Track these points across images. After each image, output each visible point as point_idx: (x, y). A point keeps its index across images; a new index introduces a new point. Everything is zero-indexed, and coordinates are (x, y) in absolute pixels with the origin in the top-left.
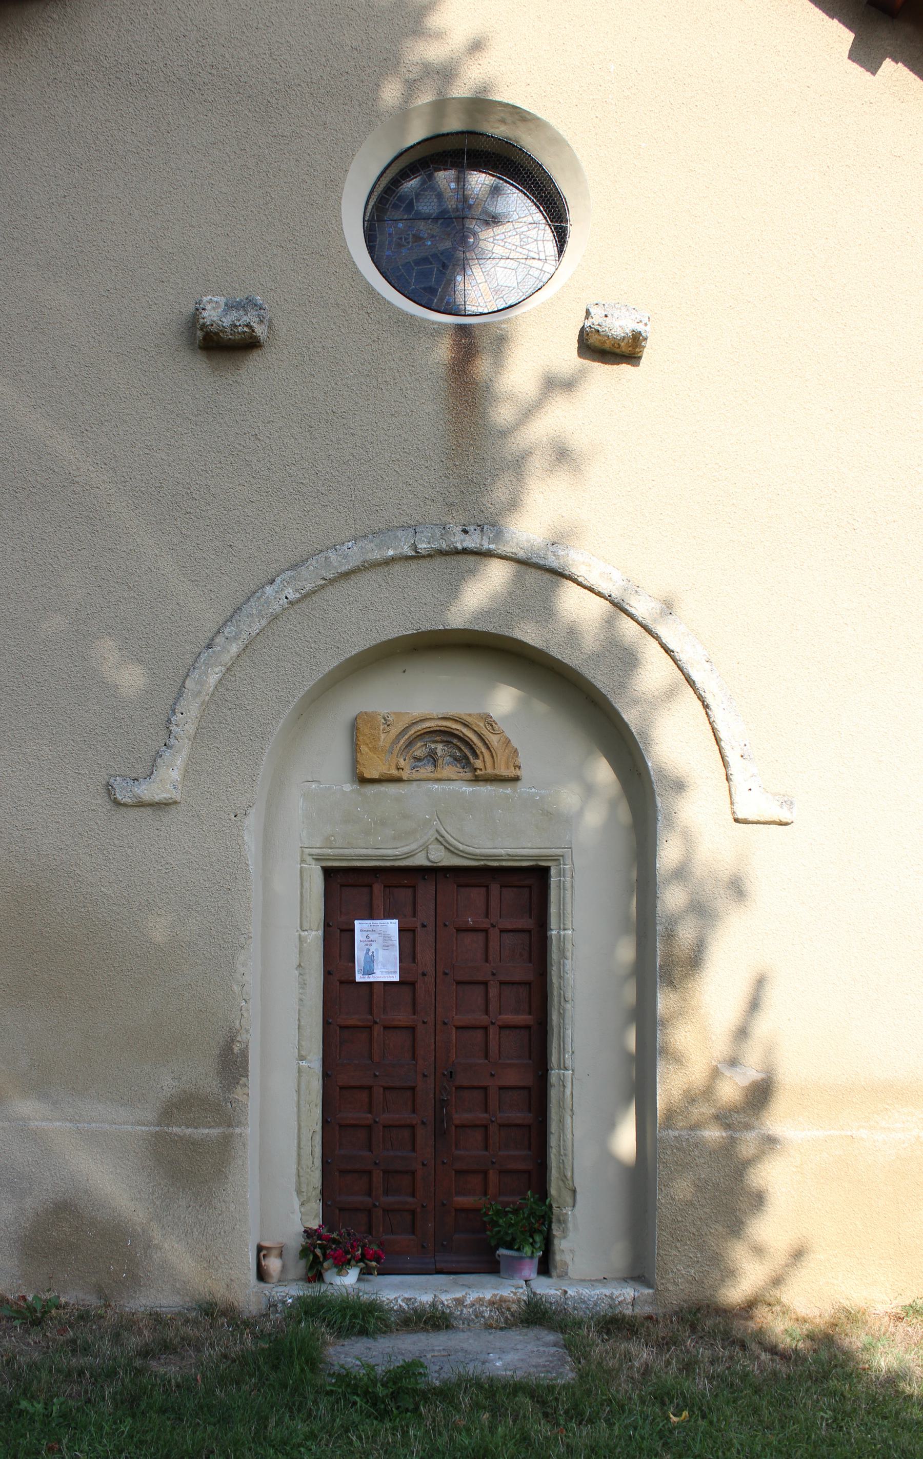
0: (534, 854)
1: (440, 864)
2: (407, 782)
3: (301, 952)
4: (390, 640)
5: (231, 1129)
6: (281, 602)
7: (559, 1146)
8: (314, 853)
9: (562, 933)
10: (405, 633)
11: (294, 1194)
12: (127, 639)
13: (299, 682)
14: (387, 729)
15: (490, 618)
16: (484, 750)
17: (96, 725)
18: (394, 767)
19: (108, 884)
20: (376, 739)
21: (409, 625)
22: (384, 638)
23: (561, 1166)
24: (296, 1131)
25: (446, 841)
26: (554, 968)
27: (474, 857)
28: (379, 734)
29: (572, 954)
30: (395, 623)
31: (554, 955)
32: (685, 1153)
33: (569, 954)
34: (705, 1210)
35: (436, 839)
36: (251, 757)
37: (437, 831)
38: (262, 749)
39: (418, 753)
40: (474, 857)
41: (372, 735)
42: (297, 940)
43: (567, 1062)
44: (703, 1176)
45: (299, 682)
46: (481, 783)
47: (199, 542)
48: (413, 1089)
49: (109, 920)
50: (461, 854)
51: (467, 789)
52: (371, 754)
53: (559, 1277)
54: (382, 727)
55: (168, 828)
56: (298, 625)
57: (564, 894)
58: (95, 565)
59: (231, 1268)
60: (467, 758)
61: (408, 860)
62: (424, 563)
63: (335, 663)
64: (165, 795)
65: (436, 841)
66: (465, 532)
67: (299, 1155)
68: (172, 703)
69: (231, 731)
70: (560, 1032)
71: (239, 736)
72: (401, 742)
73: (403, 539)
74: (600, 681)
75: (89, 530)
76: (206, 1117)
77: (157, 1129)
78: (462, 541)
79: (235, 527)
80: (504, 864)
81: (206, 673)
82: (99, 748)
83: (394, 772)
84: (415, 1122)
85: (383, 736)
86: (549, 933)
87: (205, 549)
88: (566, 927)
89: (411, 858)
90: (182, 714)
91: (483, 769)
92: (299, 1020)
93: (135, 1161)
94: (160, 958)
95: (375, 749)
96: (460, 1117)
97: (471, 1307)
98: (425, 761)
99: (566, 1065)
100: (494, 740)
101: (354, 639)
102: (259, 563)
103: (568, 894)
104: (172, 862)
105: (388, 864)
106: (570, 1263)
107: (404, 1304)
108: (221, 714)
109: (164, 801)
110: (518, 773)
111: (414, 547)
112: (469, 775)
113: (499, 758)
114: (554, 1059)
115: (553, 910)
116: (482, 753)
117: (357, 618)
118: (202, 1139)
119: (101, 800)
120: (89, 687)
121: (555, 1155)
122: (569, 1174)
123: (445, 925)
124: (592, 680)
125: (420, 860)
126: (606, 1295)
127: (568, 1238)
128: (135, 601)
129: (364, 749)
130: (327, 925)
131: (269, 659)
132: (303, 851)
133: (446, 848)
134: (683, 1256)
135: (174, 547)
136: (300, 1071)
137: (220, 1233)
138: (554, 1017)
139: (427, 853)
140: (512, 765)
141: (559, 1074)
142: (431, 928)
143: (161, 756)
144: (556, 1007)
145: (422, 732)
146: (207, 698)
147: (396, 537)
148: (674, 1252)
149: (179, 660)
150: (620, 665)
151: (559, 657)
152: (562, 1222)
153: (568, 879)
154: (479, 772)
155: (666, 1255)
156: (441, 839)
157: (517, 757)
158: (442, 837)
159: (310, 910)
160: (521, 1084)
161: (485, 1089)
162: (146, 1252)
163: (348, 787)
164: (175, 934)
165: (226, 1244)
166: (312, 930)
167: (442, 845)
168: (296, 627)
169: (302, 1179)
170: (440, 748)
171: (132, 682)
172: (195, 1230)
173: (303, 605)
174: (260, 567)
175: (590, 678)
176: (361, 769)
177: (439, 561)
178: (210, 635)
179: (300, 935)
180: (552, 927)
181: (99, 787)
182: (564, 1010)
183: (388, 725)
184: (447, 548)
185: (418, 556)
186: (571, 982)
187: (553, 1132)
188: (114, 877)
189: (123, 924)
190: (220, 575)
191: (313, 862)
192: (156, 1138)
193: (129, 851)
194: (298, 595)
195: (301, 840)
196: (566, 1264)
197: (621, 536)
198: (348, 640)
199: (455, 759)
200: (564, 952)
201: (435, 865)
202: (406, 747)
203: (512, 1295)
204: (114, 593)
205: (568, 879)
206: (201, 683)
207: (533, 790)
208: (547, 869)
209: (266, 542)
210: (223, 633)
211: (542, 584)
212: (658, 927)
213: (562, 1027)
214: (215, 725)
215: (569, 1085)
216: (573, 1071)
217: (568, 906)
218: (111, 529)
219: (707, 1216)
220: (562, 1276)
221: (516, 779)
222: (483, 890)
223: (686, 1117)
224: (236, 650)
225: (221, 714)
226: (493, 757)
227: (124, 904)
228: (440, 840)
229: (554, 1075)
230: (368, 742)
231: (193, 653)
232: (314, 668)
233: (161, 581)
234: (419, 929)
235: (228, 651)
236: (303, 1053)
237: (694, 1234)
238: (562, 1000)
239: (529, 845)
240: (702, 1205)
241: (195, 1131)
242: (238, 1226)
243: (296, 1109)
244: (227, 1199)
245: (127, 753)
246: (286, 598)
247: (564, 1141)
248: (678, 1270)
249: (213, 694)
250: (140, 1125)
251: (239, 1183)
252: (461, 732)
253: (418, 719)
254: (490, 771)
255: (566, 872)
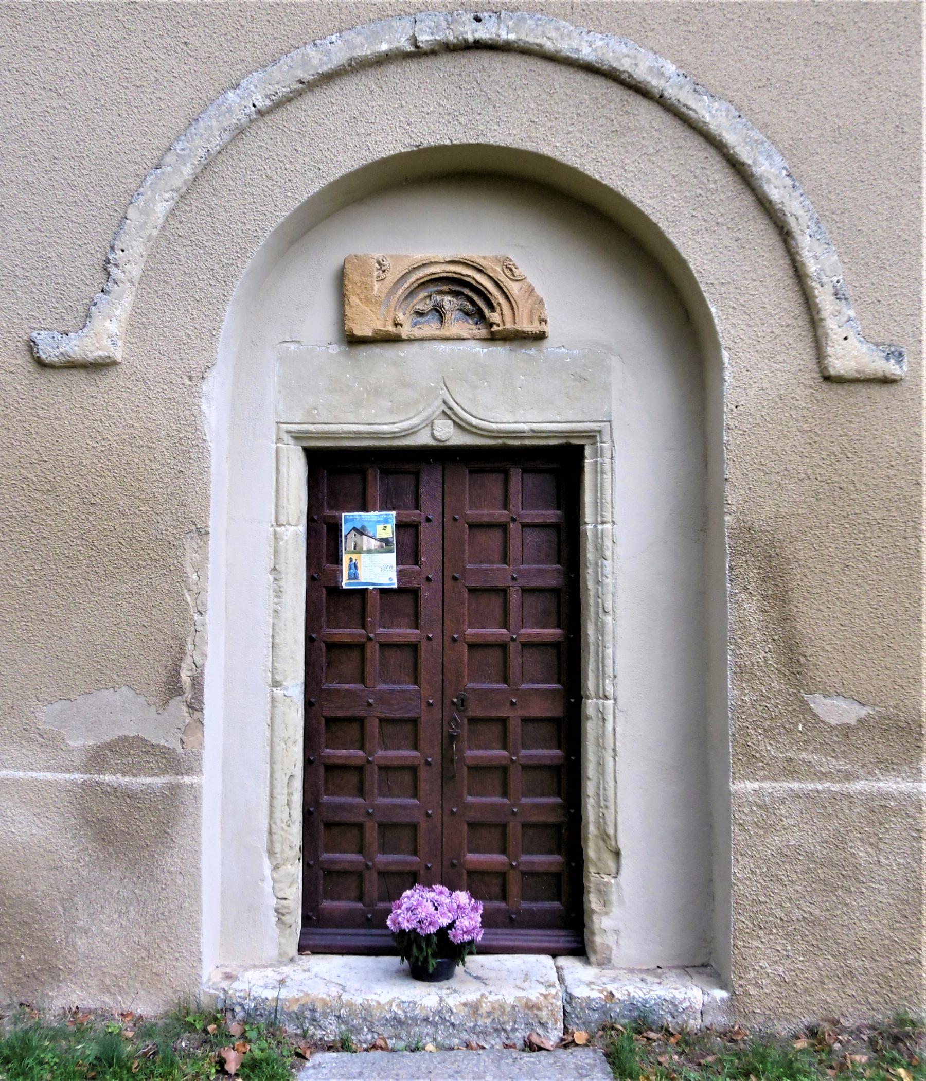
0: (564, 429)
1: (448, 443)
2: (406, 343)
3: (276, 552)
4: (384, 161)
5: (180, 777)
6: (247, 111)
7: (598, 795)
8: (292, 429)
9: (600, 527)
10: (403, 151)
11: (265, 855)
12: (55, 158)
13: (271, 213)
14: (382, 276)
15: (509, 129)
16: (502, 300)
17: (17, 265)
18: (390, 322)
19: (28, 465)
20: (368, 288)
21: (407, 140)
22: (376, 157)
23: (601, 820)
24: (268, 776)
25: (456, 414)
26: (590, 571)
27: (489, 434)
28: (372, 281)
29: (613, 553)
30: (390, 138)
31: (590, 553)
32: (768, 812)
33: (608, 553)
34: (797, 887)
35: (444, 412)
36: (210, 307)
37: (445, 402)
38: (224, 295)
39: (420, 307)
40: (490, 434)
41: (363, 283)
42: (272, 537)
43: (607, 689)
44: (793, 843)
45: (271, 213)
46: (499, 343)
47: (145, 39)
48: (415, 722)
49: (29, 509)
50: (474, 430)
51: (481, 350)
52: (363, 307)
53: (600, 964)
54: (376, 273)
55: (105, 395)
56: (269, 141)
57: (602, 479)
58: (16, 66)
59: (177, 959)
60: (480, 313)
61: (408, 438)
62: (426, 63)
63: (315, 188)
64: (100, 353)
65: (442, 416)
66: (478, 20)
67: (271, 806)
68: (111, 238)
69: (185, 273)
70: (598, 651)
71: (196, 279)
72: (400, 292)
73: (400, 30)
74: (649, 206)
75: (9, 23)
76: (149, 762)
77: (86, 777)
78: (474, 31)
79: (191, 19)
80: (527, 442)
81: (153, 200)
82: (19, 294)
83: (391, 328)
84: (417, 762)
85: (377, 285)
86: (582, 528)
87: (154, 47)
88: (605, 519)
89: (413, 436)
90: (123, 251)
91: (501, 325)
92: (273, 636)
93: (56, 818)
94: (93, 559)
95: (367, 300)
96: (474, 754)
97: (488, 1016)
98: (430, 317)
99: (607, 694)
100: (514, 288)
101: (339, 158)
102: (221, 63)
103: (607, 478)
104: (110, 438)
105: (384, 443)
106: (614, 947)
107: (399, 1012)
108: (173, 252)
109: (100, 361)
110: (543, 327)
111: (414, 41)
112: (483, 332)
113: (520, 309)
114: (590, 684)
115: (588, 497)
116: (499, 304)
117: (343, 132)
118: (142, 791)
119: (23, 360)
120: (8, 218)
121: (593, 806)
122: (611, 831)
123: (455, 519)
124: (639, 205)
125: (423, 439)
126: (665, 1000)
127: (611, 914)
128: (65, 111)
129: (353, 299)
130: (310, 520)
131: (234, 184)
132: (279, 429)
133: (454, 422)
134: (767, 948)
135: (115, 45)
136: (273, 700)
137: (163, 914)
138: (590, 631)
139: (433, 429)
140: (536, 318)
141: (597, 704)
142: (436, 523)
143: (95, 304)
144: (593, 620)
145: (426, 279)
146: (155, 233)
147: (391, 27)
148: (756, 943)
149: (120, 184)
150: (674, 185)
151: (597, 177)
152: (603, 894)
153: (607, 460)
154: (495, 328)
155: (745, 947)
156: (449, 412)
157: (543, 308)
158: (451, 409)
159: (288, 499)
160: (549, 715)
161: (504, 721)
162: (67, 938)
163: (334, 349)
164: (112, 529)
165: (170, 928)
166: (289, 524)
167: (450, 418)
168: (267, 144)
169: (275, 837)
170: (448, 301)
171: (61, 212)
172: (132, 908)
173: (277, 117)
174: (222, 69)
175: (635, 202)
176: (349, 325)
177: (446, 63)
178: (159, 154)
179: (275, 531)
180: (587, 520)
181: (19, 344)
182: (603, 623)
183: (384, 271)
184: (455, 41)
185: (418, 53)
186: (611, 588)
187: (591, 777)
188: (36, 456)
189: (47, 515)
190: (173, 79)
191: (291, 441)
192: (84, 790)
193: (56, 424)
194: (268, 103)
195: (277, 413)
196: (609, 948)
197: (675, 20)
198: (331, 159)
199: (467, 314)
200: (602, 551)
201: (442, 444)
202: (406, 298)
203: (542, 998)
204: (40, 102)
205: (607, 460)
206: (145, 212)
207: (563, 350)
208: (582, 448)
209: (229, 37)
210: (175, 150)
211: (575, 84)
212: (727, 518)
213: (601, 645)
214: (165, 266)
215: (610, 718)
216: (615, 700)
217: (608, 492)
218: (36, 23)
219: (799, 895)
220: (603, 964)
221: (540, 337)
222: (501, 477)
223: (768, 764)
224: (191, 172)
225: (173, 252)
226: (512, 309)
227: (48, 491)
228: (448, 413)
229: (590, 706)
230: (358, 291)
231: (138, 175)
232: (289, 194)
233: (98, 86)
234: (423, 524)
235: (181, 173)
236: (278, 678)
237: (781, 920)
238: (601, 610)
239: (558, 419)
240: (792, 882)
241: (134, 780)
242: (187, 904)
243: (268, 749)
244: (172, 869)
245: (54, 301)
246: (254, 106)
247: (605, 789)
248: (761, 967)
249: (163, 228)
250: (63, 772)
251: (188, 848)
252: (474, 279)
253: (420, 264)
254: (509, 326)
255: (605, 451)
